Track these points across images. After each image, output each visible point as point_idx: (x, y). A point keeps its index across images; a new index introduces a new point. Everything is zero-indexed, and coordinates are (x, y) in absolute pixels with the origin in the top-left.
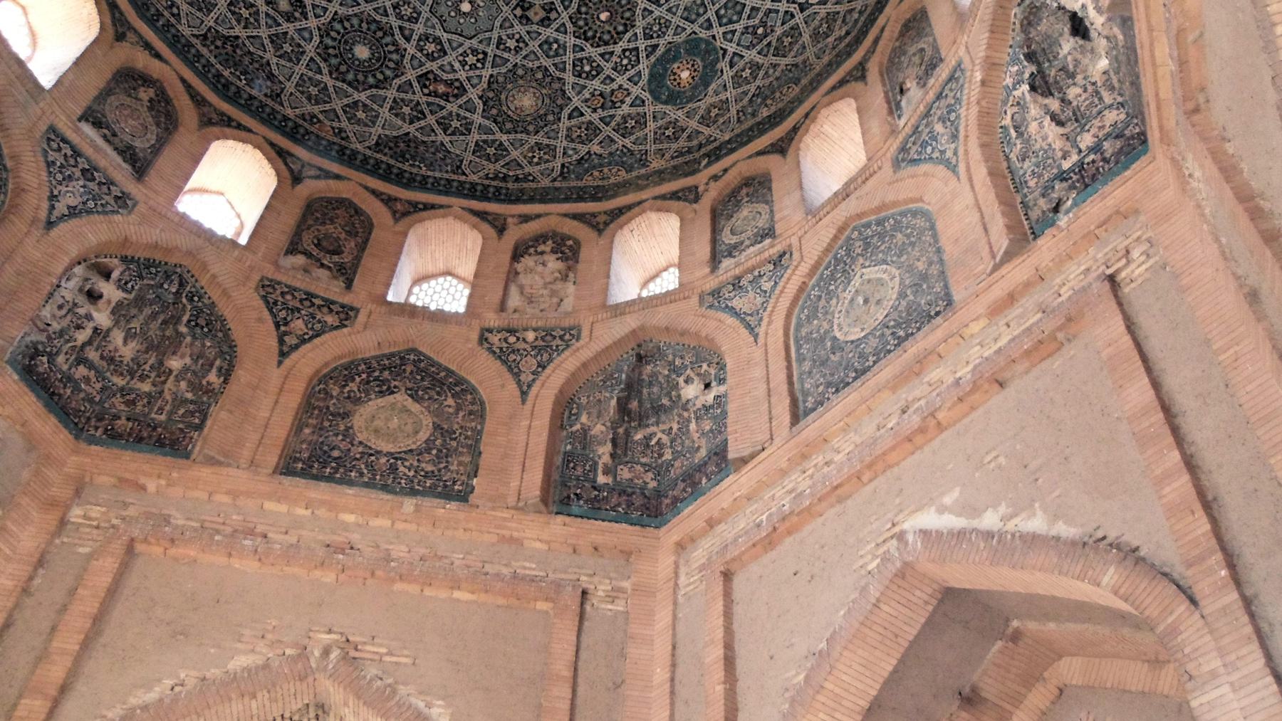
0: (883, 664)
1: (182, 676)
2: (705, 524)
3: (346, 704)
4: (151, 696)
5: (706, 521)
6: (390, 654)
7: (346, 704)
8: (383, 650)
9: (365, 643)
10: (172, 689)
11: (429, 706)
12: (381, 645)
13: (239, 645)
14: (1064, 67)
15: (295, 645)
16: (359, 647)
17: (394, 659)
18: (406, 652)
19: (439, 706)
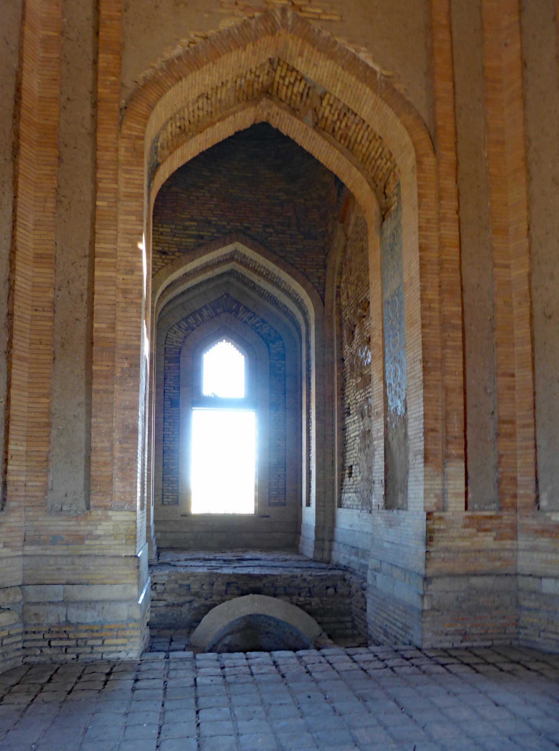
0: (297, 126)
1: (192, 36)
2: (520, 538)
3: (301, 55)
4: (179, 50)
5: (516, 539)
6: (325, 13)
7: (301, 55)
8: (319, 11)
9: (305, 6)
10: (189, 46)
11: (358, 51)
12: (316, 7)
13: (222, 11)
14: (95, 608)
15: (260, 9)
16: (303, 9)
17: (328, 17)
18: (334, 12)
19: (364, 52)
